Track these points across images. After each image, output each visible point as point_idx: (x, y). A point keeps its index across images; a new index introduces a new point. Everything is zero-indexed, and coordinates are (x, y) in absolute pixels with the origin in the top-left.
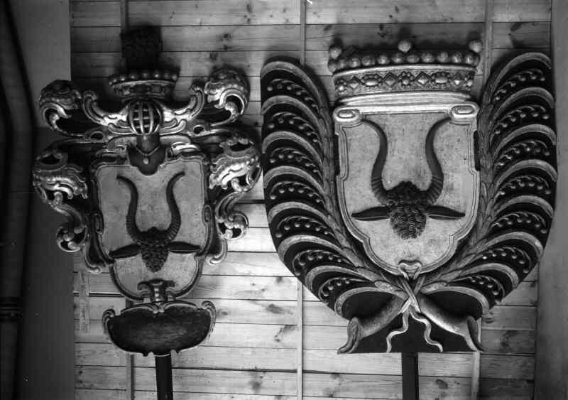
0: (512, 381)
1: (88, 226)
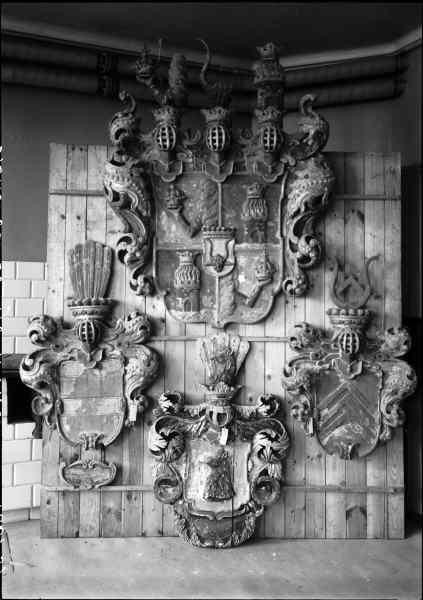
0: (78, 519)
1: (317, 256)
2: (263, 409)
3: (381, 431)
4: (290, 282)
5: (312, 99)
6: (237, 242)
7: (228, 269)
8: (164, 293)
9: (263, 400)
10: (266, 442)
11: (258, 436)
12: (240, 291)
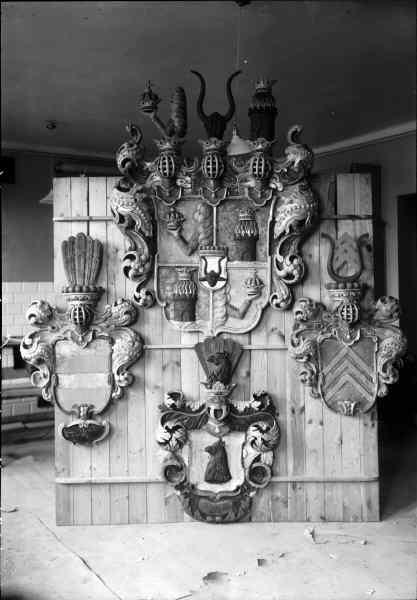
2: (256, 405)
3: (379, 388)
4: (275, 297)
5: (299, 130)
6: (228, 260)
7: (220, 284)
8: (164, 304)
9: (255, 396)
10: (257, 434)
11: (252, 428)
12: (232, 303)
